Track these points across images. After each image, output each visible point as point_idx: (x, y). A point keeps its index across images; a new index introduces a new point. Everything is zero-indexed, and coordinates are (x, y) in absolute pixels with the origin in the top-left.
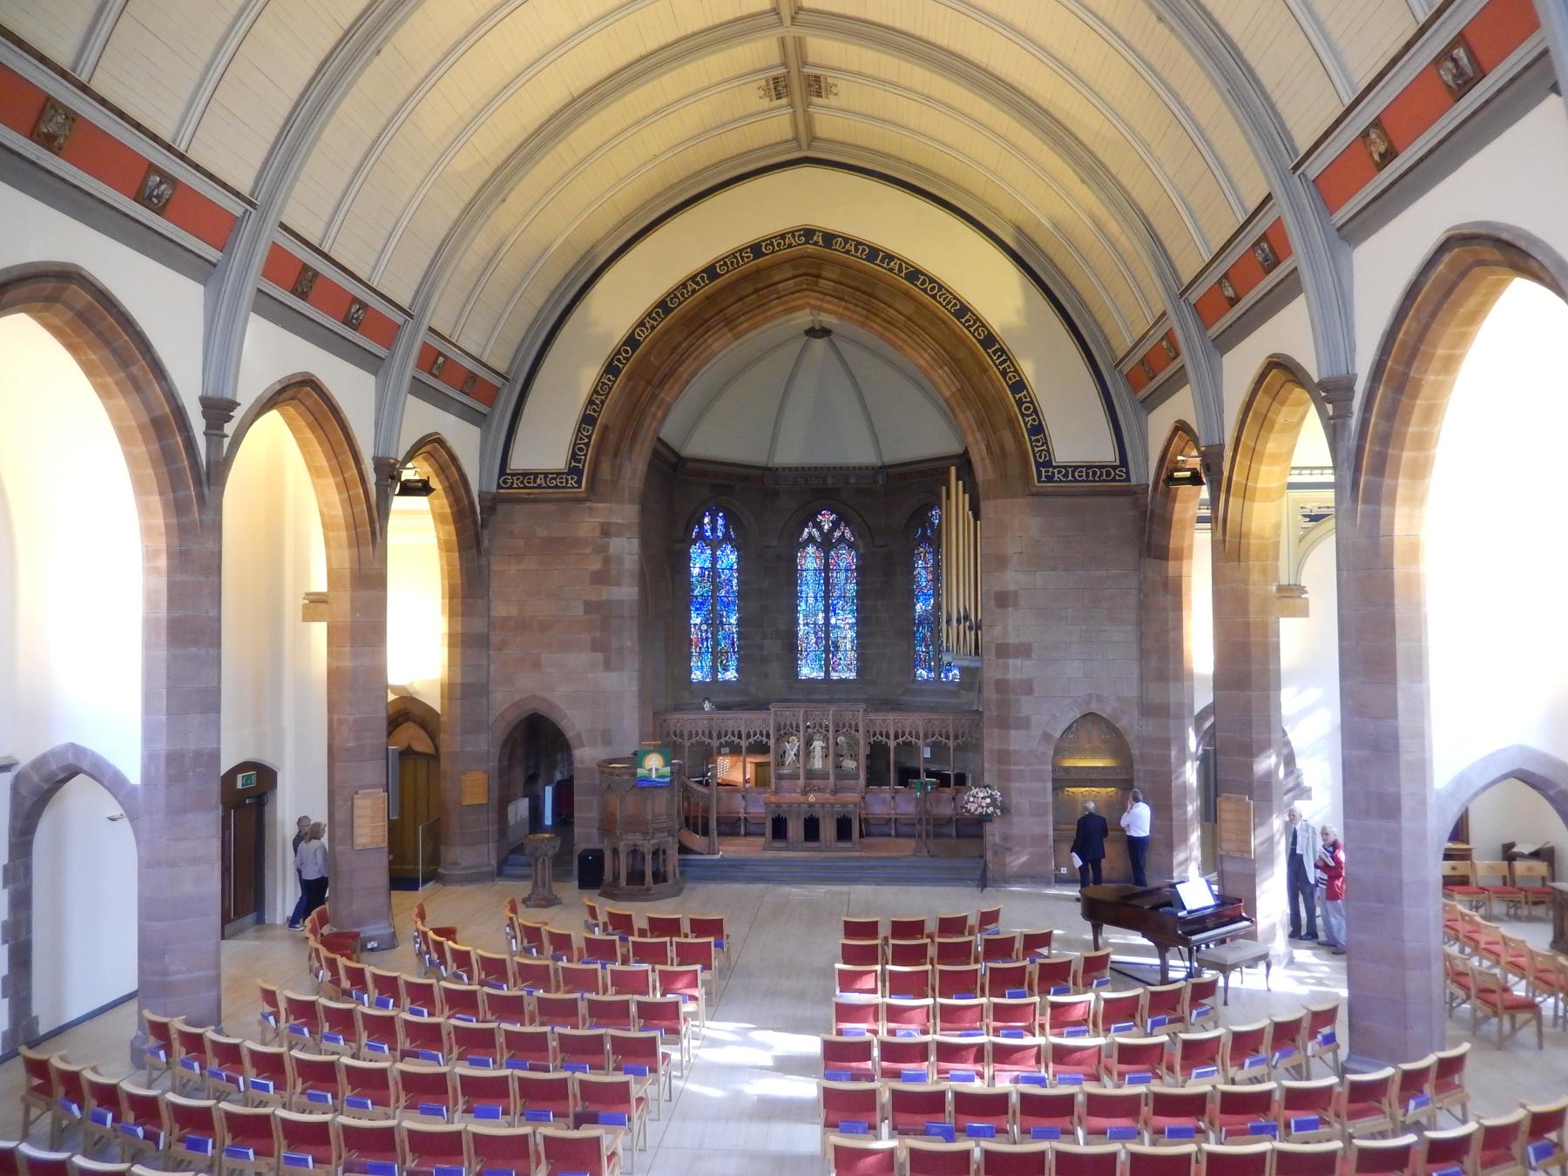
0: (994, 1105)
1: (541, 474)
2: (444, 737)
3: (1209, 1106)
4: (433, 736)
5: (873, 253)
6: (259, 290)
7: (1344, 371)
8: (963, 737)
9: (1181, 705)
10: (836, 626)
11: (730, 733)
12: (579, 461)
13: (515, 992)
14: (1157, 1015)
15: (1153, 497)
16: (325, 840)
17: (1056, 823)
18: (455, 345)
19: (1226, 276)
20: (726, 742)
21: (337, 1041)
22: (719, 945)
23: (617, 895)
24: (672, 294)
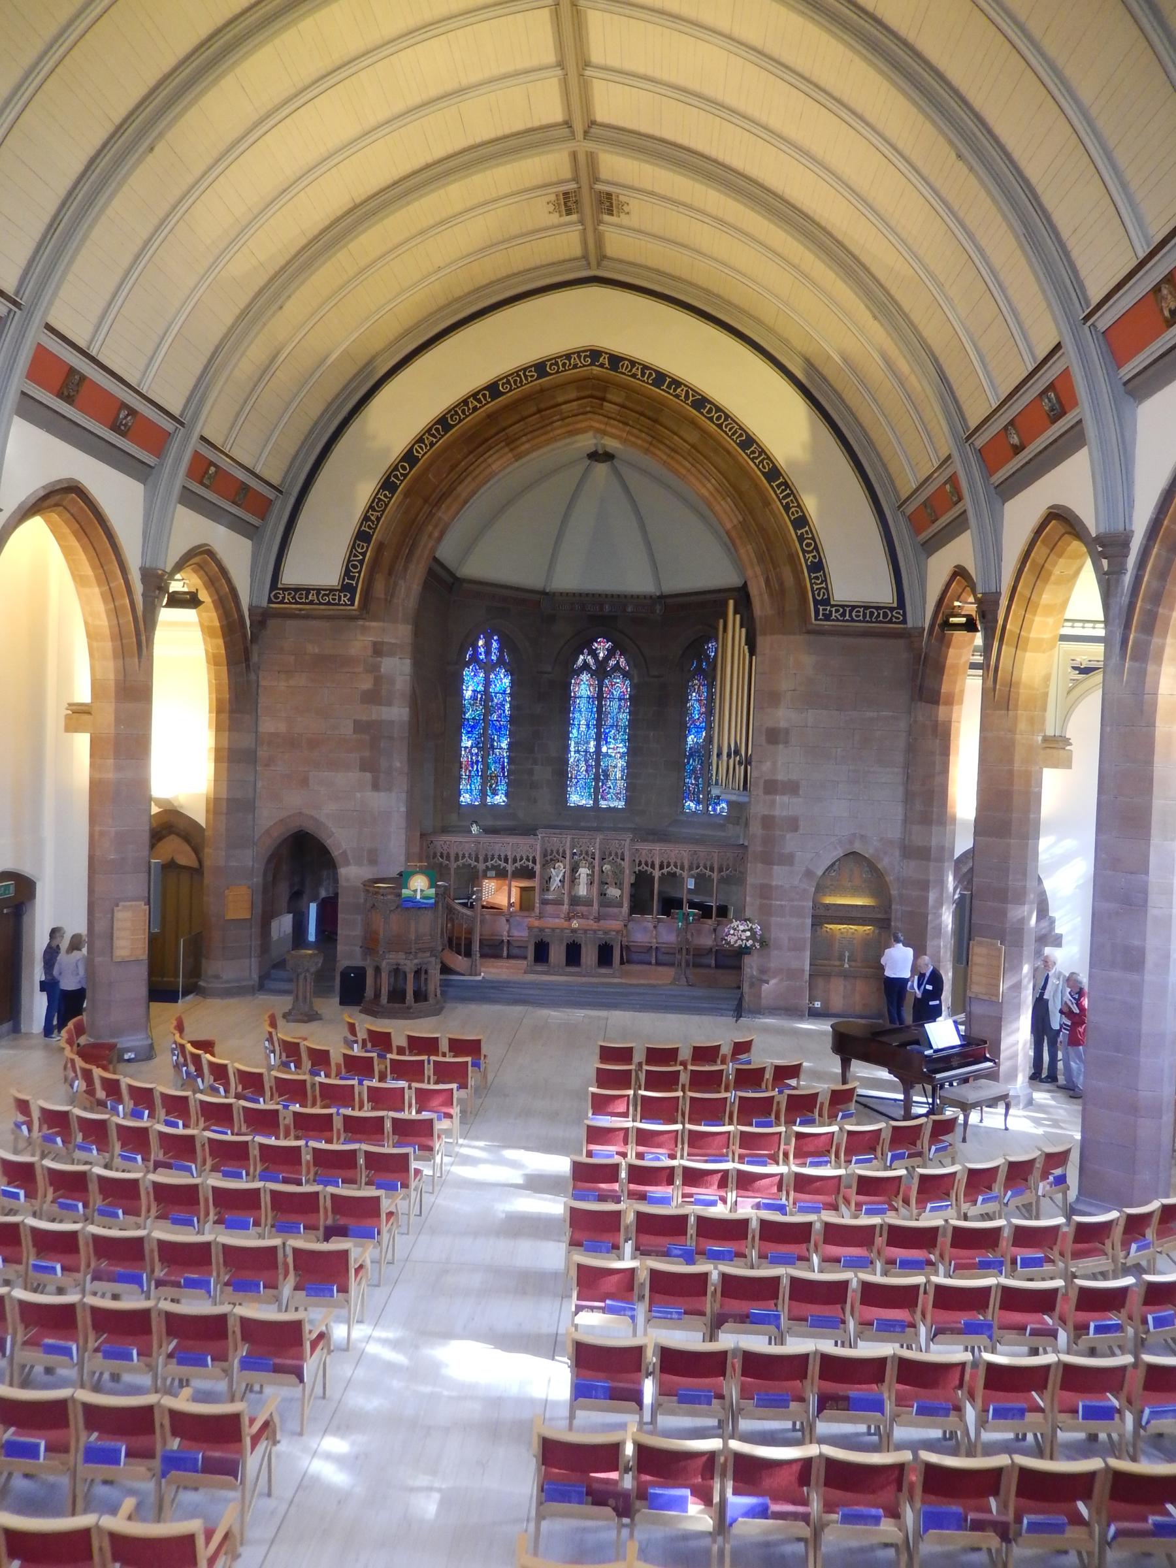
0: (734, 1229)
1: (313, 590)
2: (208, 851)
3: (940, 1239)
4: (197, 850)
5: (660, 378)
6: (23, 393)
7: (1121, 528)
8: (727, 870)
9: (942, 848)
10: (607, 755)
11: (496, 856)
12: (352, 578)
13: (271, 1106)
14: (896, 1150)
15: (929, 640)
16: (85, 950)
17: (813, 958)
18: (227, 455)
19: (1012, 423)
20: (492, 865)
21: (90, 1150)
22: (476, 1065)
23: (378, 1012)
24: (453, 411)
